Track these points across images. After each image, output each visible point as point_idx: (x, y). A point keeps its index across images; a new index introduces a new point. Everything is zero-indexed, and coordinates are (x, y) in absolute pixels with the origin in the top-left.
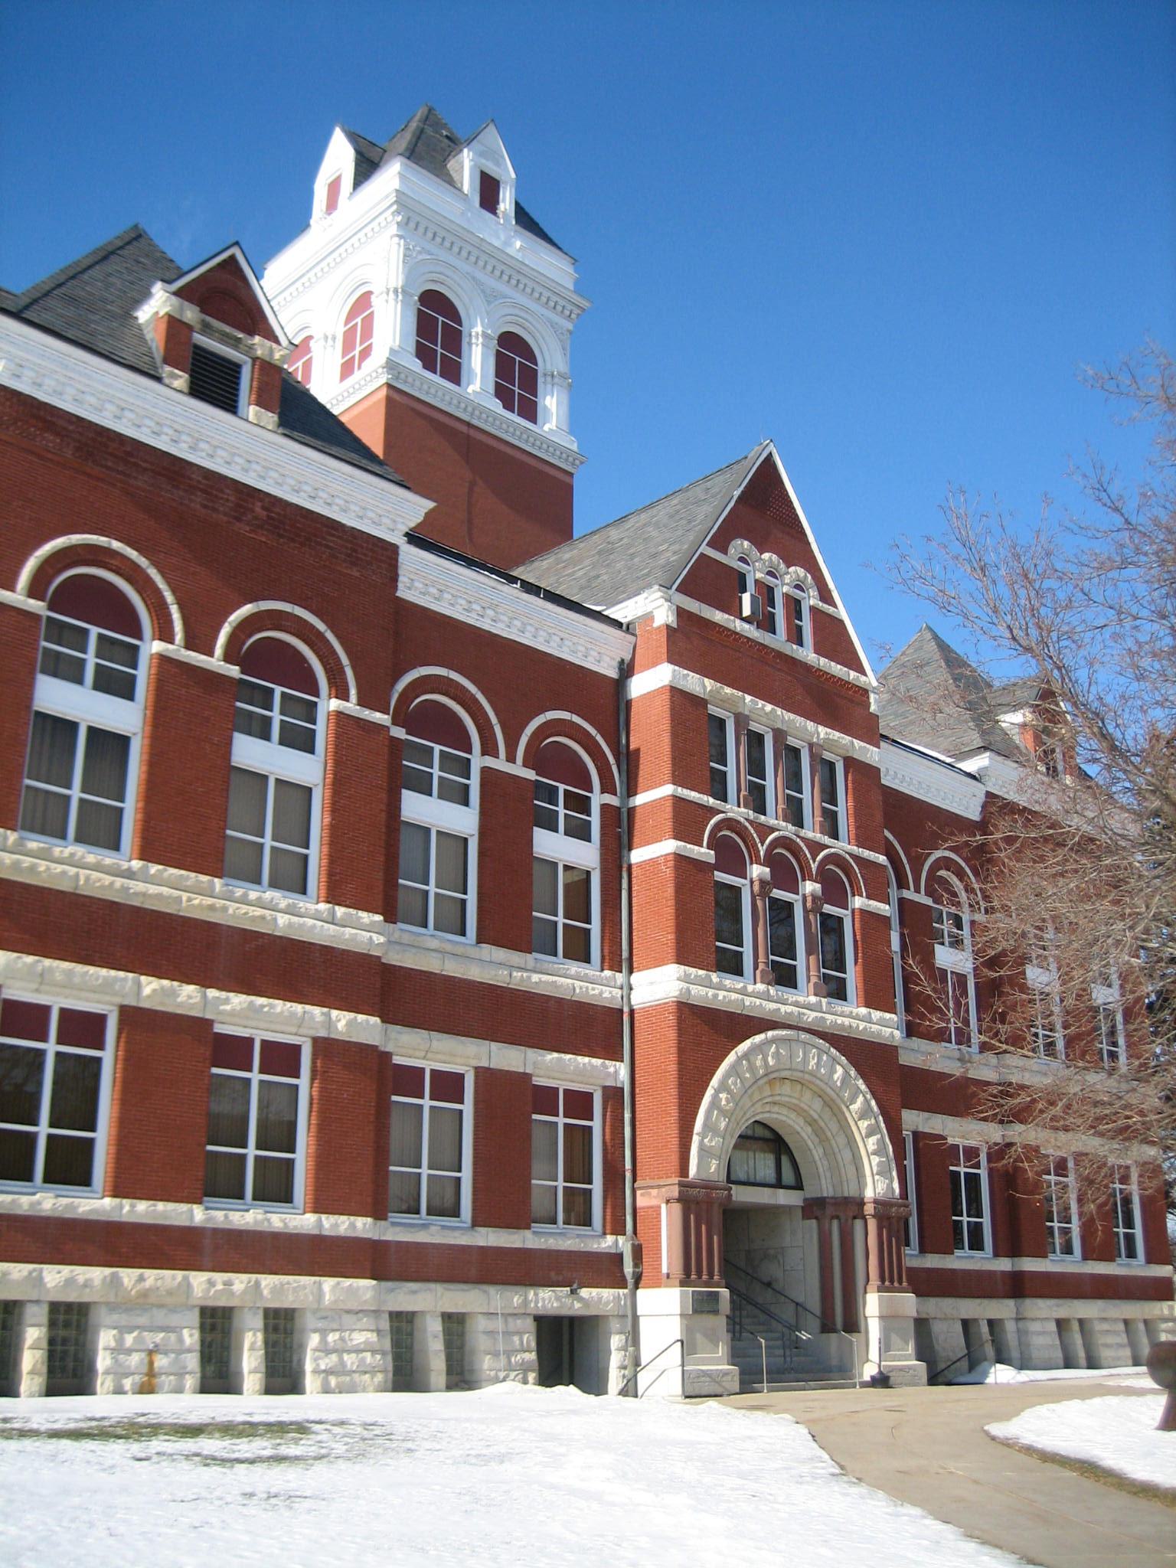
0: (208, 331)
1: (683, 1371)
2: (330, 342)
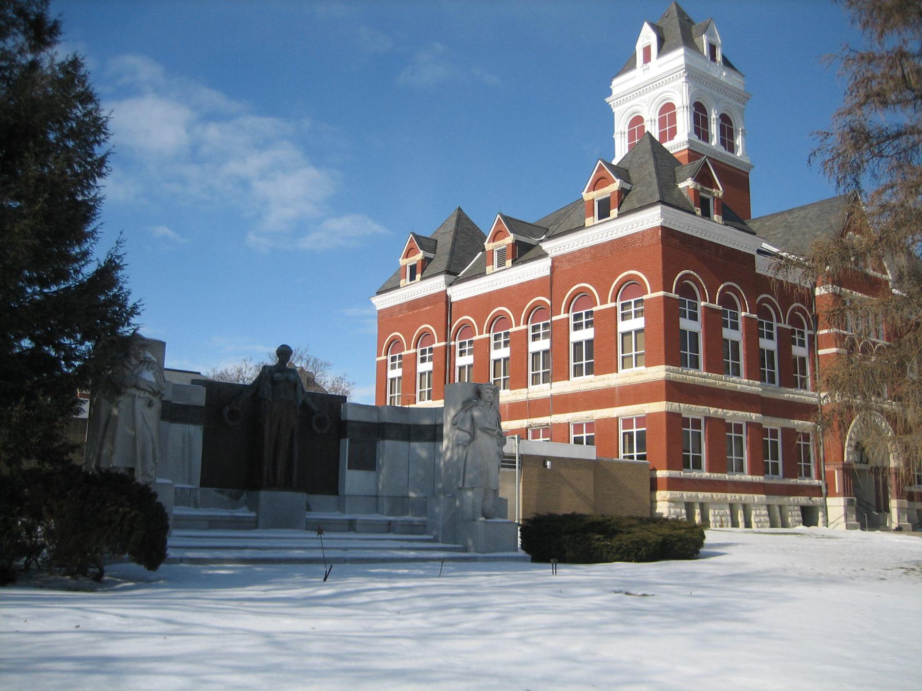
2: (653, 122)
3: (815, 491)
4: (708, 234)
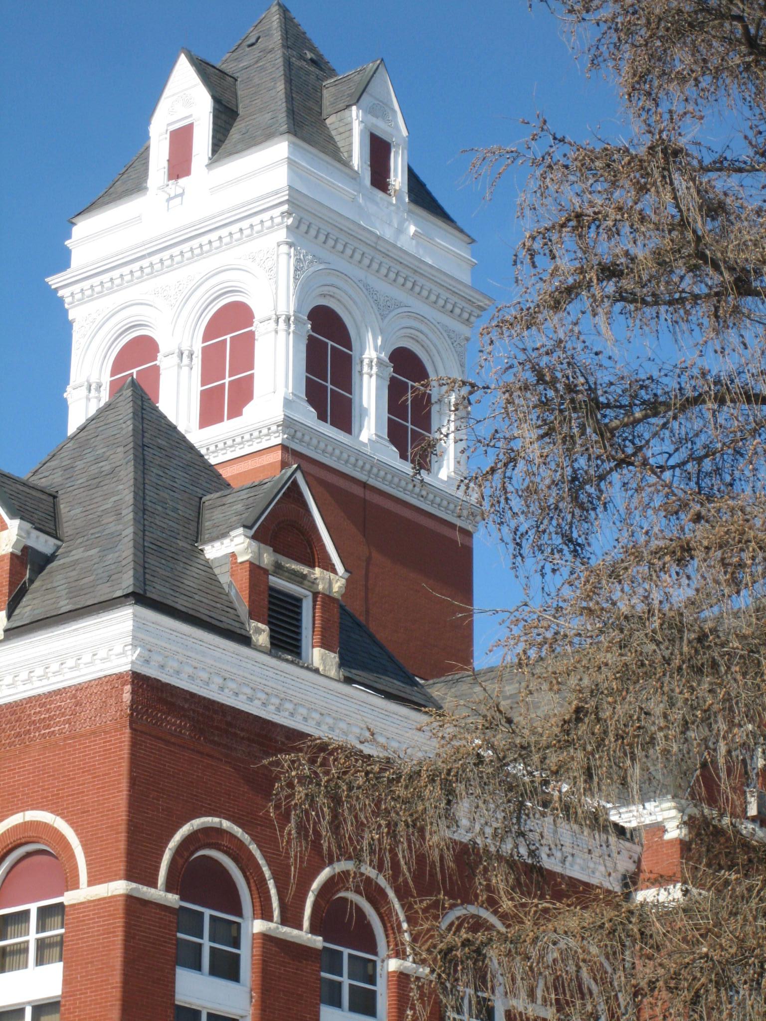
0: (281, 572)
2: (186, 360)
4: (289, 706)
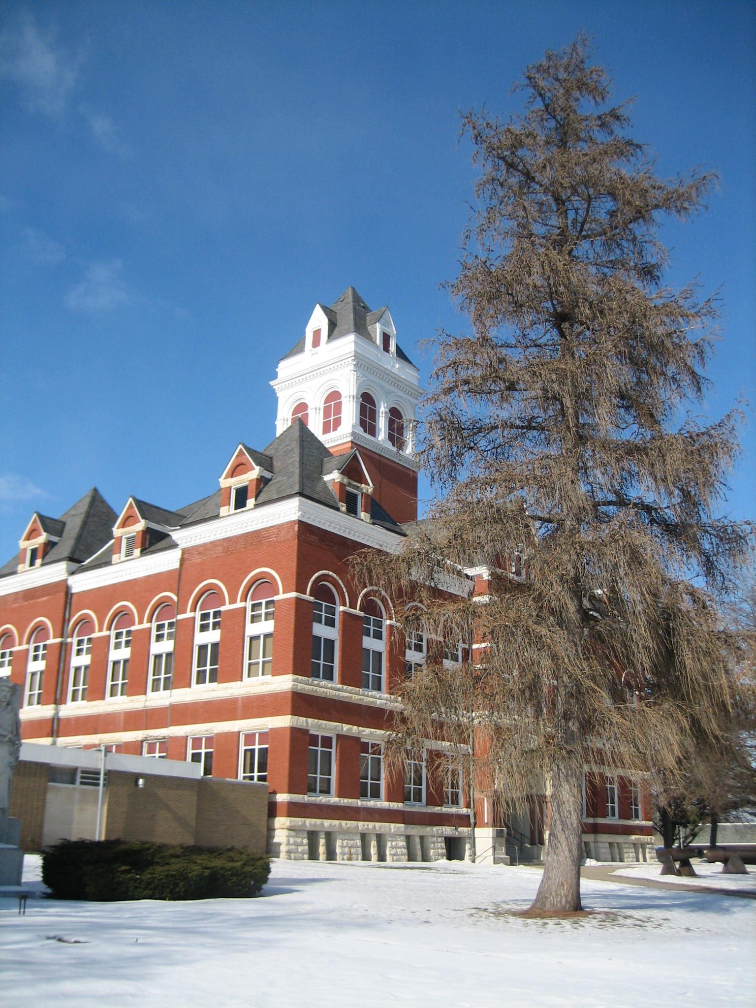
1: (494, 858)
2: (318, 411)
3: (464, 820)
